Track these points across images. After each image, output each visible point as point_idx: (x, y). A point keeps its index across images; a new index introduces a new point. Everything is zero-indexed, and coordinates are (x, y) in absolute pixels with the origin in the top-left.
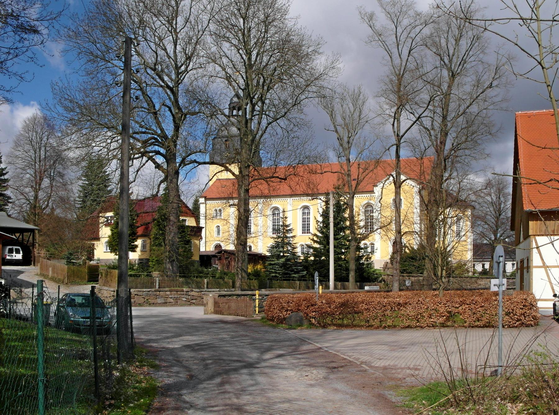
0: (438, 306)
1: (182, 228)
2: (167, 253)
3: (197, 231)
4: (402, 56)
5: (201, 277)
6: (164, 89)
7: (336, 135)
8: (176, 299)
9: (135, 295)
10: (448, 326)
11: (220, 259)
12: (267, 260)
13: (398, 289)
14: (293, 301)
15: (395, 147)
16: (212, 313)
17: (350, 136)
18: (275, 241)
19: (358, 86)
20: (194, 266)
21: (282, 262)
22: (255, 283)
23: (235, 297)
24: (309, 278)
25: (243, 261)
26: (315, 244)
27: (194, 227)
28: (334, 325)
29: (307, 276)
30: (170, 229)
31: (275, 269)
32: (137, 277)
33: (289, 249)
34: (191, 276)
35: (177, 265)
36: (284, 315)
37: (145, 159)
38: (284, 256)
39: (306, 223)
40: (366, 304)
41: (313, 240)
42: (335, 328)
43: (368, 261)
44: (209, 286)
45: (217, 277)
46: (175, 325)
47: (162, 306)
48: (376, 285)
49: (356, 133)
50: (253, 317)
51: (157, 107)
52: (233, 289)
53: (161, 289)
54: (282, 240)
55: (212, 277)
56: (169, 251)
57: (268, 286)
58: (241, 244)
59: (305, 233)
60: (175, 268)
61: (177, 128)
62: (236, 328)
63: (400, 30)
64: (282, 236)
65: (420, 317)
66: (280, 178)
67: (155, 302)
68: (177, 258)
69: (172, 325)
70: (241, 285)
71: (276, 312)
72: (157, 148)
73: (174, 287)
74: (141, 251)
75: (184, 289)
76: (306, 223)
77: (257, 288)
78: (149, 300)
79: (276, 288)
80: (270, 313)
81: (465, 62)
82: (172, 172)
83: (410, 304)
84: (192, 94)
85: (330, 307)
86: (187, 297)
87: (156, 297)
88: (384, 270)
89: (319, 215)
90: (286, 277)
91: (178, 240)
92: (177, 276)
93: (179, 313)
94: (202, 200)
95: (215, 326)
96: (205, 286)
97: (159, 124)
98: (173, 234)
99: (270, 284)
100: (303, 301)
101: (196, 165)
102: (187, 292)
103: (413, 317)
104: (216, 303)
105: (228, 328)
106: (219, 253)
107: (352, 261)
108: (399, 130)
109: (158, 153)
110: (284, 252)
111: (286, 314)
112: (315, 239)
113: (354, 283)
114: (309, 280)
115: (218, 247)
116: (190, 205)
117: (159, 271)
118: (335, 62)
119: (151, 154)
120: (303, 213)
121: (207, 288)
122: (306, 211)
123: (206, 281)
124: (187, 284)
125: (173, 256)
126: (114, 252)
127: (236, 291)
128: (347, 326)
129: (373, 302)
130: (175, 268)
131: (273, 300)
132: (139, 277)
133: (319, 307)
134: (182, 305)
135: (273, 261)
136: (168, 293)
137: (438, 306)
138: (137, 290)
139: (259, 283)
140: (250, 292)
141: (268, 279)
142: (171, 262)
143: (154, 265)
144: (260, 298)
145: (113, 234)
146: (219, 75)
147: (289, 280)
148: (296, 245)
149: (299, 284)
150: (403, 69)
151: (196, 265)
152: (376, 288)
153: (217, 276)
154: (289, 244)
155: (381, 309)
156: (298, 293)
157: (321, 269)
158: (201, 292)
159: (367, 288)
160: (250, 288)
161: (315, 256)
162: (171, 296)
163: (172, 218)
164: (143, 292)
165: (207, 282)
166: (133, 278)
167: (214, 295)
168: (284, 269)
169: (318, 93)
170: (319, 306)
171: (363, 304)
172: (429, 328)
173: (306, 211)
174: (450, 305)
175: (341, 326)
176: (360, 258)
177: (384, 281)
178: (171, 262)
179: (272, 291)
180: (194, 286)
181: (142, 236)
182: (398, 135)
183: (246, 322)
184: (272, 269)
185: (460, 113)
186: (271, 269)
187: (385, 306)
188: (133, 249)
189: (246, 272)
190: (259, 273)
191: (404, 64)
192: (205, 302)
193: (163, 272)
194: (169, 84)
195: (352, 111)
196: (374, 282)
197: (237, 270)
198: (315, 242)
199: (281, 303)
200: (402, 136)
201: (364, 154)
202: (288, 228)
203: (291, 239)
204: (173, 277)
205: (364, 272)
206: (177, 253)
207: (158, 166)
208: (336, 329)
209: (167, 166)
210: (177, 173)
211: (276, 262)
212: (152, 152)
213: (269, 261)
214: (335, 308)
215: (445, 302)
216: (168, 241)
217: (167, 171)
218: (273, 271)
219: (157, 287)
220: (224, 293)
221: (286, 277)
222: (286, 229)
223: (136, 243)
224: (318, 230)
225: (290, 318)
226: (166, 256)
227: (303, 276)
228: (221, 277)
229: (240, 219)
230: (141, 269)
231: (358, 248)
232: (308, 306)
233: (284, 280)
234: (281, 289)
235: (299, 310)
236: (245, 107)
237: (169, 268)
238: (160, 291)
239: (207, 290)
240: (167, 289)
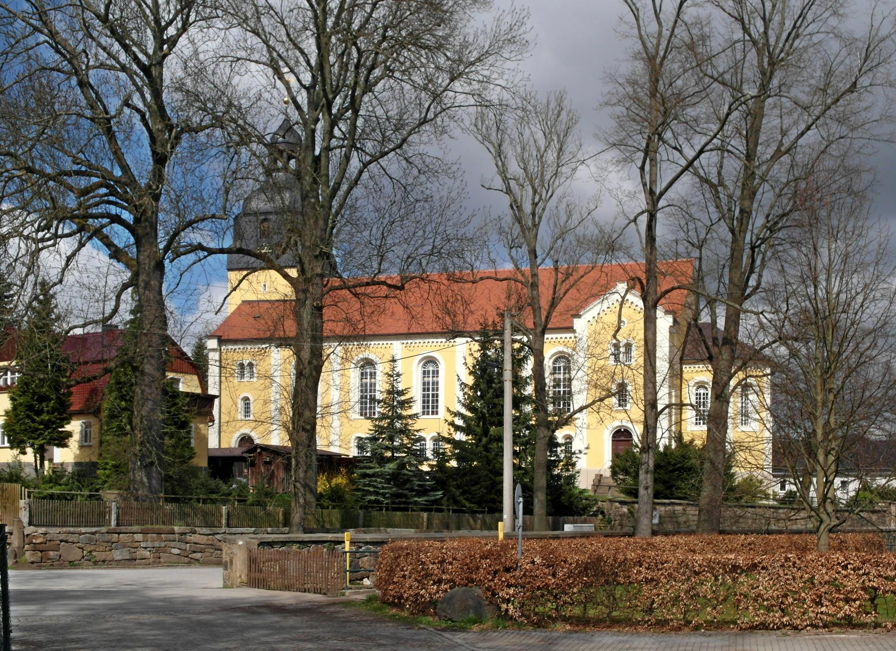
0: (839, 573)
1: (170, 394)
2: (138, 448)
4: (661, 16)
5: (213, 501)
8: (158, 551)
9: (61, 541)
10: (863, 626)
11: (253, 464)
12: (356, 467)
13: (649, 531)
14: (454, 559)
16: (242, 585)
17: (536, 200)
18: (375, 426)
19: (558, 93)
20: (197, 477)
21: (391, 471)
22: (335, 515)
23: (295, 547)
24: (448, 506)
25: (309, 467)
26: (458, 433)
28: (566, 620)
29: (444, 501)
30: (143, 392)
31: (374, 487)
32: (66, 499)
33: (405, 442)
34: (191, 499)
35: (160, 474)
36: (430, 594)
38: (392, 459)
39: (431, 392)
40: (648, 569)
41: (452, 424)
42: (568, 627)
43: (568, 470)
44: (231, 522)
45: (248, 502)
46: (154, 618)
47: (124, 567)
48: (585, 522)
50: (343, 595)
52: (287, 529)
53: (123, 529)
54: (389, 424)
55: (239, 501)
56: (142, 443)
57: (361, 522)
58: (304, 429)
59: (428, 414)
60: (154, 482)
61: (160, 160)
62: (311, 627)
64: (390, 414)
65: (791, 600)
66: (389, 286)
67: (108, 558)
68: (160, 459)
69: (145, 618)
70: (304, 519)
71: (409, 587)
72: (113, 210)
73: (152, 524)
74: (81, 447)
75: (176, 528)
76: (431, 392)
77: (338, 526)
78: (94, 553)
79: (379, 526)
80: (391, 587)
81: (797, 36)
82: (148, 264)
83: (763, 568)
85: (554, 575)
86: (183, 546)
87: (111, 545)
88: (595, 491)
89: (468, 371)
90: (400, 503)
91: (161, 417)
92: (159, 498)
93: (163, 585)
94: (212, 344)
95: (257, 621)
96: (224, 522)
97: (118, 157)
98: (150, 404)
99: (365, 517)
100: (481, 558)
101: (202, 254)
102: (182, 534)
103: (773, 602)
104: (252, 562)
105: (292, 627)
106: (251, 451)
107: (541, 471)
108: (653, 182)
109: (116, 219)
110: (394, 449)
111: (437, 592)
112: (459, 422)
113: (544, 517)
114: (449, 510)
115: (246, 440)
116: (188, 351)
117: (120, 489)
118: (516, 27)
120: (424, 372)
122: (431, 369)
123: (224, 509)
124: (183, 516)
125: (151, 453)
126: (18, 447)
127: (293, 533)
128: (598, 623)
129: (666, 562)
130: (154, 482)
131: (399, 556)
132: (72, 499)
133: (524, 575)
134: (170, 565)
135: (370, 468)
136: (139, 537)
137: (839, 573)
138: (64, 529)
139: (342, 516)
140: (330, 536)
141: (361, 508)
142: (145, 467)
143: (108, 476)
144: (354, 549)
145: (15, 408)
146: (256, 57)
147: (406, 509)
148: (420, 434)
149: (428, 519)
150: (663, 47)
151: (203, 476)
152: (588, 527)
153: (250, 499)
154: (405, 431)
155: (688, 579)
156: (452, 539)
157: (473, 485)
158: (214, 534)
159: (568, 528)
160: (323, 526)
161: (459, 458)
162: (145, 544)
163: (148, 368)
164: (80, 534)
165: (228, 513)
166: (57, 503)
167: (247, 543)
168: (396, 485)
169: (476, 97)
170: (527, 570)
171: (641, 566)
172: (815, 631)
173: (431, 369)
174: (873, 571)
175: (582, 622)
176: (552, 465)
177: (602, 513)
178: (145, 467)
179: (370, 532)
180: (197, 522)
181: (79, 414)
182: (651, 192)
183: (332, 609)
184: (369, 485)
185: (783, 149)
186: (365, 485)
187: (697, 573)
188: (62, 440)
189: (313, 491)
190: (340, 494)
191: (666, 33)
192: (225, 558)
193: (128, 491)
195: (543, 149)
196: (581, 515)
197: (295, 487)
198: (457, 428)
199: (423, 563)
200: (662, 194)
201: (567, 242)
202: (403, 398)
203: (410, 422)
204: (151, 502)
205: (562, 494)
206: (160, 447)
207: (116, 254)
208: (570, 632)
209: (138, 251)
210: (160, 267)
211: (378, 470)
213: (361, 468)
214: (569, 577)
215: (858, 563)
216: (138, 419)
217: (138, 263)
218: (371, 489)
219: (113, 523)
220: (273, 537)
221: (400, 503)
222: (399, 398)
223: (68, 428)
224: (463, 405)
225: (449, 600)
226: (135, 455)
227: (435, 502)
228: (259, 501)
229: (299, 375)
230: (76, 483)
231: (552, 444)
232: (496, 572)
233: (395, 509)
234: (389, 530)
235: (472, 581)
236: (313, 126)
237: (142, 482)
238: (119, 534)
239: (228, 530)
240: (135, 528)
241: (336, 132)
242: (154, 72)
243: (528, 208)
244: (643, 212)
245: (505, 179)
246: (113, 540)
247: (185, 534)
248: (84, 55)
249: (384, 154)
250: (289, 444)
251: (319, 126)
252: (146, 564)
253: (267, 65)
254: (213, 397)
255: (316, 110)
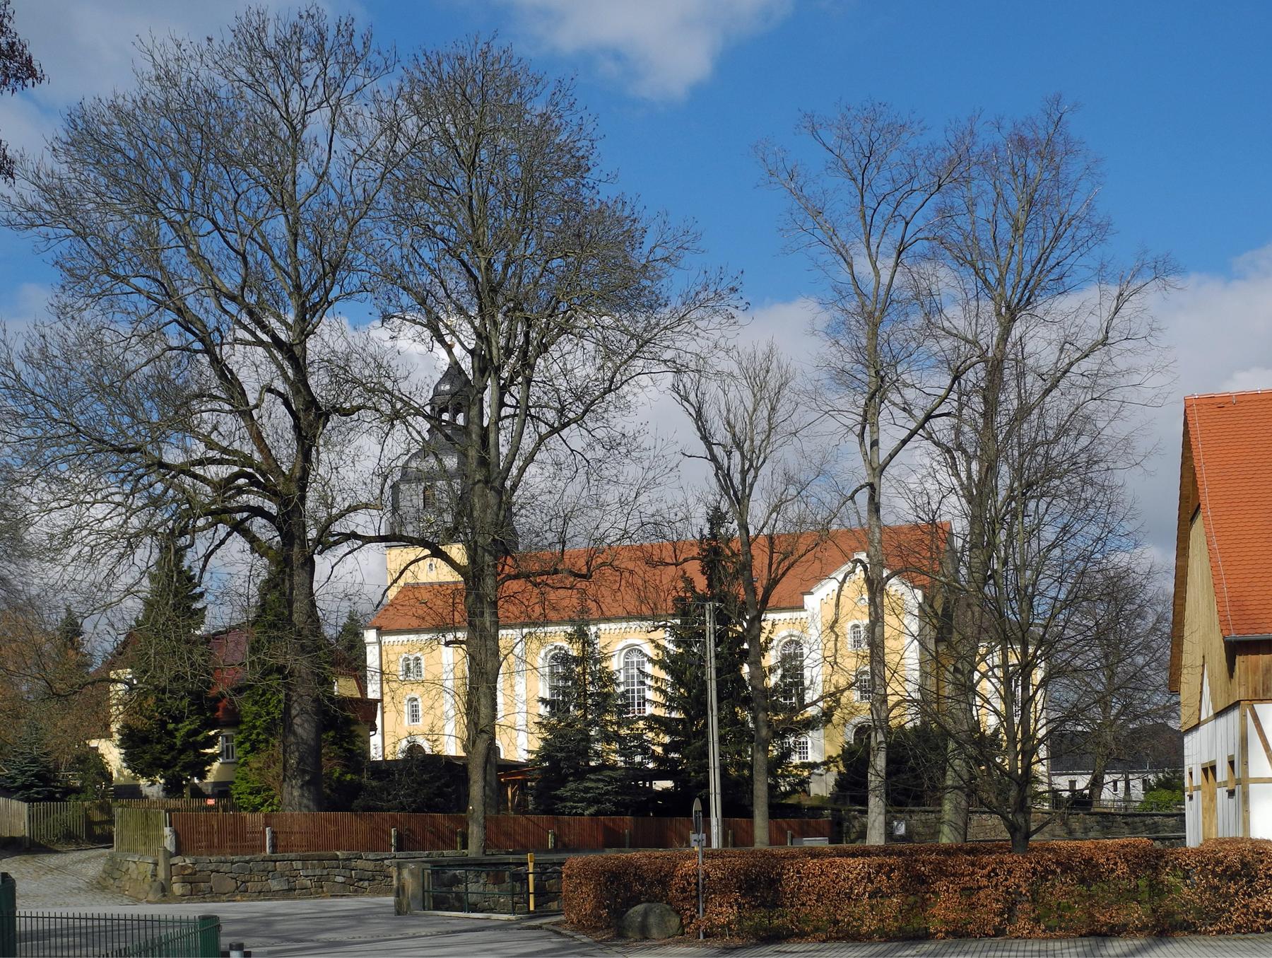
3: (367, 711)
6: (269, 352)
7: (710, 468)
9: (212, 872)
15: (866, 491)
27: (352, 700)
37: (222, 529)
49: (761, 460)
51: (252, 399)
53: (278, 855)
63: (870, 202)
72: (254, 500)
84: (340, 370)
119: (238, 516)
121: (398, 849)
122: (635, 659)
164: (233, 863)
194: (283, 337)
195: (751, 409)
212: (241, 509)
241: (508, 399)
242: (297, 350)
243: (737, 478)
244: (862, 487)
245: (709, 445)
246: (270, 868)
247: (350, 859)
248: (217, 334)
249: (564, 426)
250: (463, 754)
251: (487, 392)
252: (306, 893)
253: (425, 326)
254: (375, 702)
255: (483, 377)
